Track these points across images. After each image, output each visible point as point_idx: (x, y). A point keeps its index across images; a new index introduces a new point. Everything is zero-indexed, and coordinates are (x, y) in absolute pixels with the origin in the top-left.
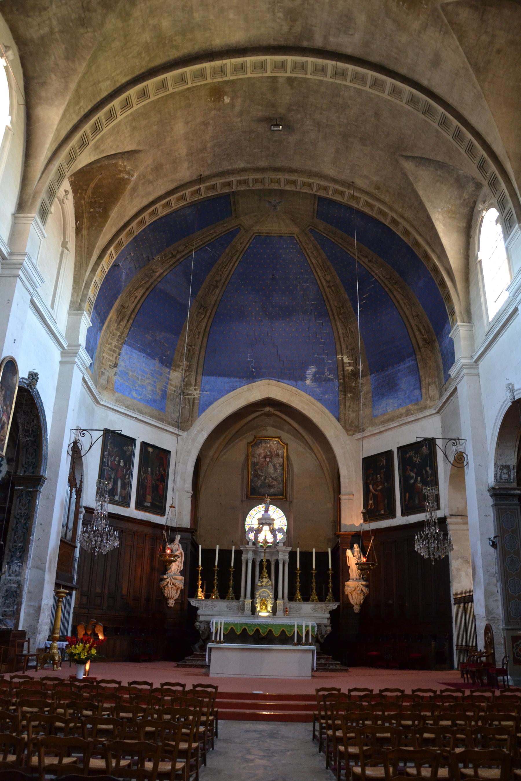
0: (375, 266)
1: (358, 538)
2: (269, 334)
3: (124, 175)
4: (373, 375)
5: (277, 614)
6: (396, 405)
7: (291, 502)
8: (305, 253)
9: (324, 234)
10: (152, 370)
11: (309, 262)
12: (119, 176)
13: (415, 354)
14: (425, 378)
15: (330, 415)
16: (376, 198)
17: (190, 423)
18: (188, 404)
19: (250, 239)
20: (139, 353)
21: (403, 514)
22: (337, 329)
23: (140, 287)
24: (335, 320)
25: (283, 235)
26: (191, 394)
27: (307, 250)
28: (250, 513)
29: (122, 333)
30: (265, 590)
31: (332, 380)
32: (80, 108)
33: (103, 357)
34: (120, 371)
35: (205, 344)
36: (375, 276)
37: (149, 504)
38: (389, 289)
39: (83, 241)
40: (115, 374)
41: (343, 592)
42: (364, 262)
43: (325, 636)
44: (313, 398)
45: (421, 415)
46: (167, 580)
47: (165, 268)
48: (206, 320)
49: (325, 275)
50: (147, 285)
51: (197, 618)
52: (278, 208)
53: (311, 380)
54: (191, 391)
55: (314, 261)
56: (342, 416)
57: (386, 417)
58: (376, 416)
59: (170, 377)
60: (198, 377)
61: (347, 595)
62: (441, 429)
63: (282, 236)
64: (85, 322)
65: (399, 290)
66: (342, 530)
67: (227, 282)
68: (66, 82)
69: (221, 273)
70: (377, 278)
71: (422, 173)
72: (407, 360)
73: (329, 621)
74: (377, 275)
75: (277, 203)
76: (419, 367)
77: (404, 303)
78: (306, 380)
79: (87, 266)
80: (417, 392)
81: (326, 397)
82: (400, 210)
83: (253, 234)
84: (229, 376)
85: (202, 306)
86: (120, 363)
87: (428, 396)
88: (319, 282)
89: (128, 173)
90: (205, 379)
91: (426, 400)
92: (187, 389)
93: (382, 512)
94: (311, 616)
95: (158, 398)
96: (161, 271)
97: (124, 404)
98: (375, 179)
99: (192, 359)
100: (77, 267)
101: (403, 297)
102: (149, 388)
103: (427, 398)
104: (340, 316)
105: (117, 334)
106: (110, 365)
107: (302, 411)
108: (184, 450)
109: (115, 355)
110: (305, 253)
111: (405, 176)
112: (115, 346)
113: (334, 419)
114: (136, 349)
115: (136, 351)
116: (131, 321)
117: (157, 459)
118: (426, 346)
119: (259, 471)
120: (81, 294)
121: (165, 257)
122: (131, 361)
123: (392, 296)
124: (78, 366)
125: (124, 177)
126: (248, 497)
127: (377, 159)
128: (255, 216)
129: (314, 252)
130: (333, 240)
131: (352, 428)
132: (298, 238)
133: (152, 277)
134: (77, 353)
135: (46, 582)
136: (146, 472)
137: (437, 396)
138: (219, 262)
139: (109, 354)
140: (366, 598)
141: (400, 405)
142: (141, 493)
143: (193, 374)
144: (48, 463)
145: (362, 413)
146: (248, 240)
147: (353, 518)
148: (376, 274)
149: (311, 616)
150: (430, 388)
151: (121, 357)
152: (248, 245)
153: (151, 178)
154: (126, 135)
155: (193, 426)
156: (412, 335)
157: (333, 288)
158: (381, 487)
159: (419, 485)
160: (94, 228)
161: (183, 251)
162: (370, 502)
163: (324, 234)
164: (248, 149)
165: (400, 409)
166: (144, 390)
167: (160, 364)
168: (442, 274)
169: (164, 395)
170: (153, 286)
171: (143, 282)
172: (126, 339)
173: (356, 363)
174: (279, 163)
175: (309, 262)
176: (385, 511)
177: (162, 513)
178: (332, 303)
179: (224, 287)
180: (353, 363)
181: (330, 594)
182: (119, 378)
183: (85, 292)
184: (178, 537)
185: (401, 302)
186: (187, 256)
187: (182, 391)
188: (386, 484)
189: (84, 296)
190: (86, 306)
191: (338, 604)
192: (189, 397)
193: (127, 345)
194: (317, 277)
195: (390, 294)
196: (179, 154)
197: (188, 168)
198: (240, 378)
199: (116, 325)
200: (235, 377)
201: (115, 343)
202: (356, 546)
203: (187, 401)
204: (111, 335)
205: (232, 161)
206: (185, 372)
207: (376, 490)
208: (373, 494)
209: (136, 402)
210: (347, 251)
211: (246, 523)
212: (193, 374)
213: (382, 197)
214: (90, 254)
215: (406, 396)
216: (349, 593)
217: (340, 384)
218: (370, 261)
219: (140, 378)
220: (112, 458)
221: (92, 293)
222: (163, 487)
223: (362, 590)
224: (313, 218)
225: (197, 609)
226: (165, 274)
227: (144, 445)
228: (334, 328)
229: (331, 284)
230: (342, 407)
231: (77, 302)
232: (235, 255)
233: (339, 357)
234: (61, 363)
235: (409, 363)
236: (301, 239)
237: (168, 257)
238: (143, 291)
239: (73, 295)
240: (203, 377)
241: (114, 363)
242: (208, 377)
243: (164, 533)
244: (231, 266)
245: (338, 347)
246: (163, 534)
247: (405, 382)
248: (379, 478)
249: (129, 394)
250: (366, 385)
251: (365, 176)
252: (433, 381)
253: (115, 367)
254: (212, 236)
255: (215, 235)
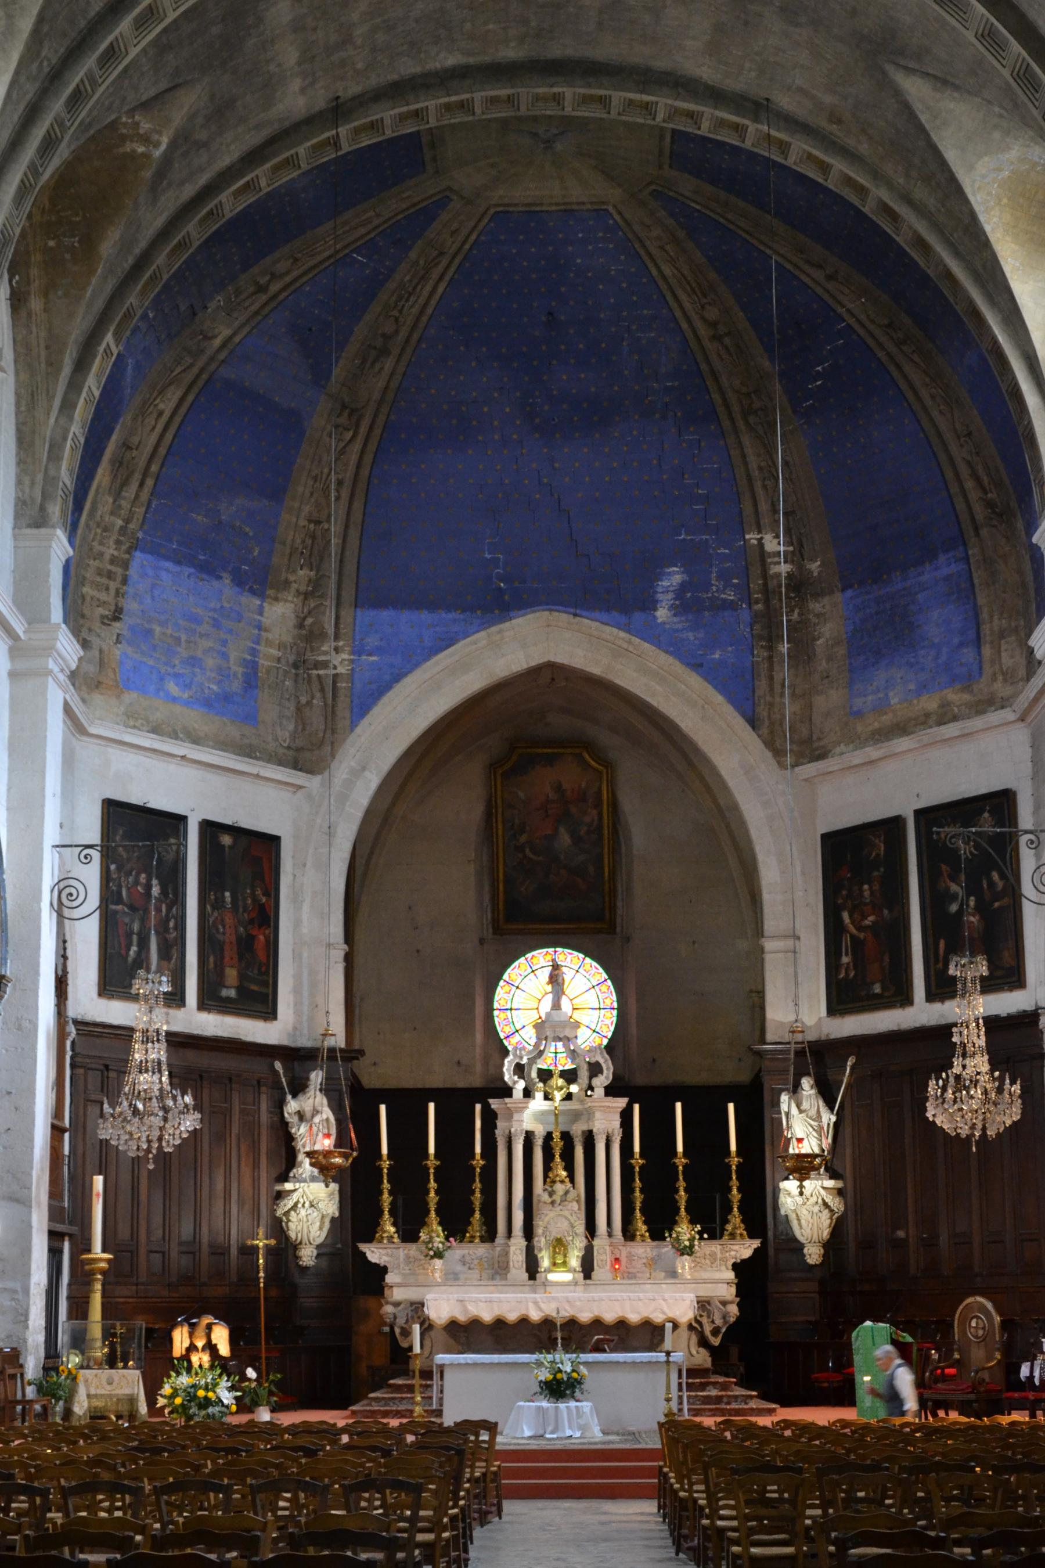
0: (846, 291)
1: (818, 1060)
2: (545, 480)
3: (135, 145)
4: (849, 593)
5: (594, 1275)
6: (912, 687)
7: (628, 939)
8: (642, 252)
9: (693, 205)
10: (215, 610)
11: (654, 272)
12: (121, 150)
13: (965, 544)
14: (991, 616)
15: (728, 710)
16: (834, 143)
17: (329, 748)
18: (318, 695)
19: (480, 220)
20: (178, 569)
21: (931, 997)
22: (744, 456)
23: (170, 384)
24: (736, 431)
25: (574, 207)
26: (325, 665)
27: (648, 243)
28: (506, 976)
29: (127, 521)
30: (560, 1218)
31: (732, 606)
32: (41, 63)
33: (83, 597)
34: (131, 628)
35: (357, 516)
36: (846, 316)
37: (232, 993)
38: (888, 354)
39: (34, 330)
40: (118, 641)
41: (776, 1207)
42: (813, 279)
43: (724, 1330)
44: (677, 663)
45: (977, 723)
46: (295, 1197)
47: (237, 324)
48: (357, 446)
49: (703, 307)
50: (189, 377)
51: (387, 1292)
52: (559, 147)
53: (672, 607)
54: (326, 653)
55: (668, 271)
56: (762, 711)
57: (886, 719)
58: (859, 714)
59: (263, 620)
60: (343, 613)
61: (787, 1216)
62: (1030, 764)
63: (572, 211)
64: (59, 547)
65: (916, 358)
66: (769, 1037)
67: (416, 336)
68: (10, 17)
69: (396, 313)
70: (852, 321)
71: (952, 106)
72: (942, 558)
73: (733, 1290)
74: (853, 315)
75: (556, 135)
76: (976, 581)
77: (933, 397)
78: (655, 609)
79: (51, 398)
80: (968, 654)
81: (717, 656)
82: (901, 181)
83: (488, 209)
84: (432, 606)
85: (344, 406)
86: (130, 605)
87: (997, 667)
88: (684, 325)
89: (146, 140)
90: (366, 616)
91: (994, 678)
92: (312, 650)
93: (877, 989)
94: (687, 1284)
95: (236, 686)
96: (227, 332)
97: (148, 722)
98: (828, 99)
99: (321, 559)
100: (24, 403)
101: (927, 380)
102: (210, 662)
103: (995, 674)
104: (752, 419)
105: (113, 525)
106: (103, 617)
107: (649, 699)
108: (313, 825)
109: (113, 585)
110: (642, 252)
111: (907, 109)
112: (113, 561)
113: (739, 723)
114: (167, 558)
115: (168, 565)
116: (150, 482)
117: (245, 860)
118: (995, 522)
119: (527, 851)
120: (40, 477)
121: (236, 297)
122: (156, 593)
123: (895, 374)
124: (56, 680)
125: (134, 151)
126: (498, 930)
127: (828, 56)
128: (493, 165)
129: (668, 248)
130: (721, 220)
131: (799, 745)
132: (620, 213)
133: (202, 351)
134: (53, 648)
135: (34, 1231)
136: (218, 904)
137: (1022, 672)
138: (391, 285)
139: (98, 586)
140: (838, 1228)
141: (923, 688)
142: (212, 965)
143: (330, 604)
144: (10, 941)
145: (820, 702)
146: (472, 224)
147: (797, 1003)
148: (848, 311)
149: (687, 1284)
150: (1003, 647)
151: (129, 589)
152: (473, 237)
153: (203, 136)
154: (145, 69)
155: (337, 757)
156: (954, 489)
157: (727, 340)
158: (872, 918)
159: (972, 919)
160: (60, 293)
161: (287, 273)
162: (845, 960)
163: (693, 205)
164: (468, 26)
165: (924, 698)
166: (197, 670)
167: (237, 589)
168: (1013, 372)
169: (252, 679)
170: (205, 376)
171: (179, 369)
172: (140, 535)
173: (797, 555)
174: (556, 51)
175: (654, 272)
176: (882, 988)
177: (269, 1013)
178: (725, 382)
179: (409, 351)
180: (793, 552)
181: (735, 1218)
182: (129, 650)
183: (52, 473)
184: (317, 1077)
185: (924, 393)
186: (298, 284)
187: (298, 654)
188: (886, 912)
189: (50, 481)
190: (55, 510)
191: (756, 1243)
192: (321, 672)
193: (143, 551)
194: (678, 314)
195: (892, 368)
196: (279, 65)
197: (303, 91)
198: (464, 611)
199: (111, 500)
200: (449, 609)
201: (110, 551)
202: (806, 1083)
203: (316, 686)
204: (99, 531)
205: (422, 55)
206: (306, 599)
207: (859, 928)
208: (852, 936)
209: (178, 709)
210: (762, 248)
211: (496, 1005)
212: (327, 603)
213: (850, 142)
214: (54, 365)
215: (940, 661)
216: (789, 1213)
217: (756, 617)
218: (830, 278)
219: (184, 638)
220: (131, 879)
221: (66, 475)
222: (267, 940)
223: (825, 1204)
224: (660, 167)
225: (383, 1270)
226: (237, 339)
227: (210, 829)
228: (735, 453)
229: (722, 329)
230: (762, 685)
231: (32, 499)
232: (437, 264)
233: (752, 537)
234: (13, 675)
235: (946, 566)
236: (628, 216)
237: (242, 297)
238: (179, 394)
239: (19, 482)
240: (359, 612)
241: (113, 608)
242: (373, 613)
243: (278, 1065)
244: (425, 293)
245: (747, 508)
246: (276, 1073)
247: (938, 621)
248: (867, 894)
249: (158, 690)
250: (832, 618)
251: (800, 90)
252: (1013, 624)
253: (116, 619)
254: (370, 227)
255: (376, 222)
